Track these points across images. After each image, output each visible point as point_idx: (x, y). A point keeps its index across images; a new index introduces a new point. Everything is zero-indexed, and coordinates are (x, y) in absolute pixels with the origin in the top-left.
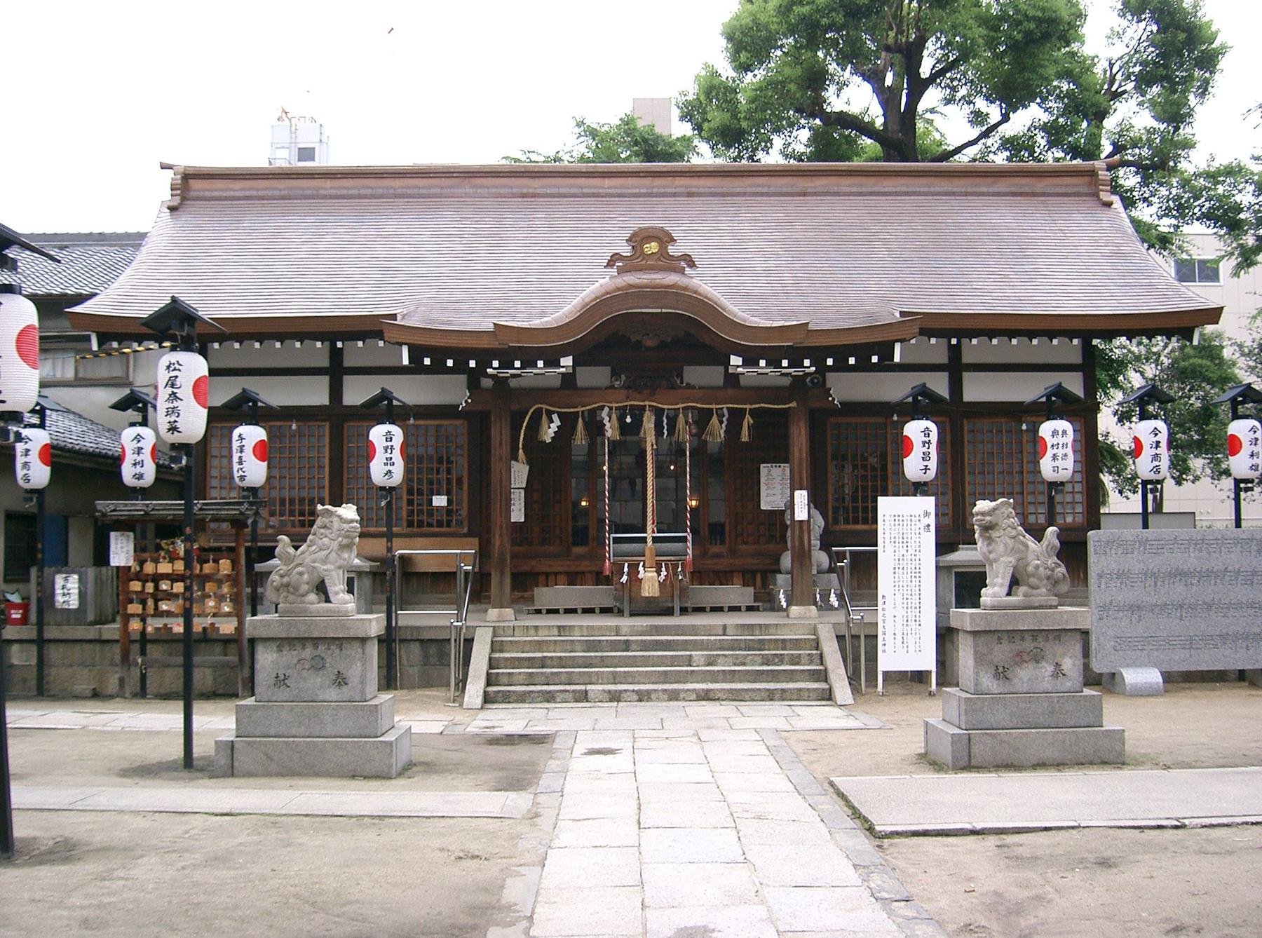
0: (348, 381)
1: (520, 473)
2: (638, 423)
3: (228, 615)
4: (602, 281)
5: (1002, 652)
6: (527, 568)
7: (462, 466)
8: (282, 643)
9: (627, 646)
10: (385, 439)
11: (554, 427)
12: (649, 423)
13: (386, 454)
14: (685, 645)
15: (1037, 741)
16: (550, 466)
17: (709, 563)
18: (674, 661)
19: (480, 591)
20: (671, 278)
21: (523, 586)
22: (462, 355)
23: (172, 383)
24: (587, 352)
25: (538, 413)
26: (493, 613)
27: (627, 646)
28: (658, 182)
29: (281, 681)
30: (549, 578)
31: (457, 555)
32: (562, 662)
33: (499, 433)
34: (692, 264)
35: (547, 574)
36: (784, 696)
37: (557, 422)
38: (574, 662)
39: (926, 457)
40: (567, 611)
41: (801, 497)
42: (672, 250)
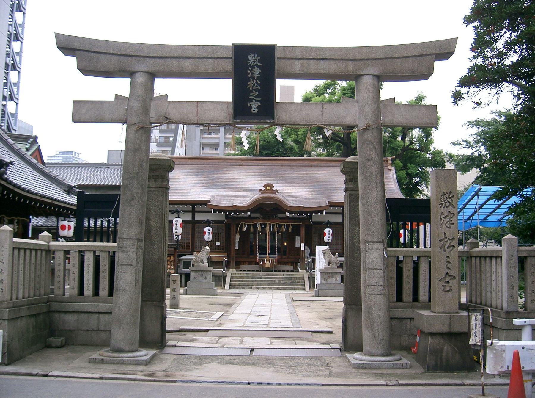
0: (196, 214)
1: (238, 237)
2: (265, 226)
3: (172, 269)
4: (257, 195)
5: (326, 276)
6: (238, 260)
7: (223, 235)
8: (196, 271)
9: (261, 278)
10: (208, 230)
11: (246, 227)
12: (268, 227)
13: (208, 233)
14: (274, 278)
15: (331, 292)
16: (244, 236)
17: (283, 260)
18: (271, 281)
19: (228, 265)
20: (273, 195)
21: (238, 265)
22: (225, 211)
23: (176, 224)
24: (252, 211)
25: (242, 224)
26: (231, 270)
27: (261, 278)
28: (274, 162)
29: (195, 278)
30: (244, 263)
31: (224, 256)
32: (246, 281)
33: (233, 229)
34: (278, 192)
35: (244, 262)
36: (295, 289)
37: (246, 226)
38: (249, 281)
39: (329, 237)
40: (248, 271)
41: (303, 245)
42: (274, 189)
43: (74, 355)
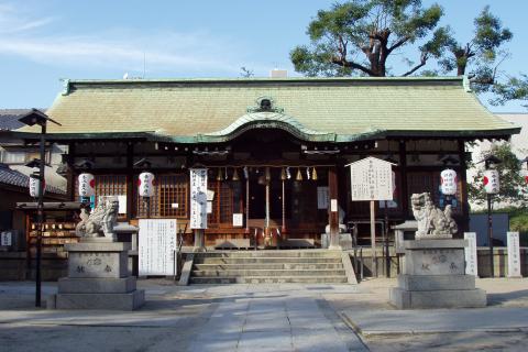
14: (281, 261)
43: (315, 337)
